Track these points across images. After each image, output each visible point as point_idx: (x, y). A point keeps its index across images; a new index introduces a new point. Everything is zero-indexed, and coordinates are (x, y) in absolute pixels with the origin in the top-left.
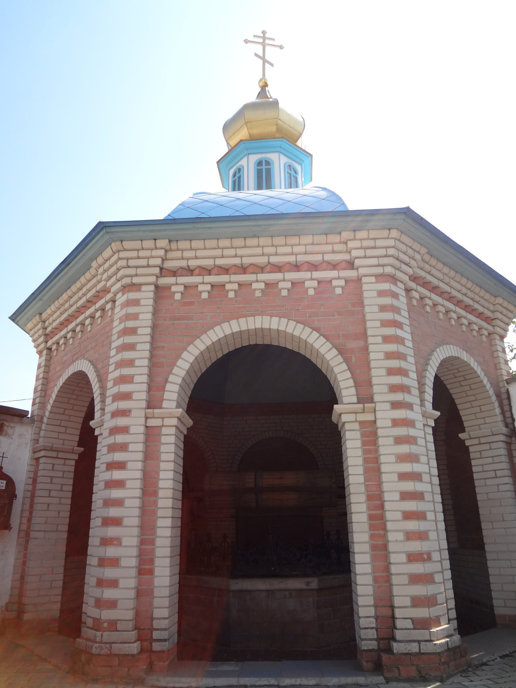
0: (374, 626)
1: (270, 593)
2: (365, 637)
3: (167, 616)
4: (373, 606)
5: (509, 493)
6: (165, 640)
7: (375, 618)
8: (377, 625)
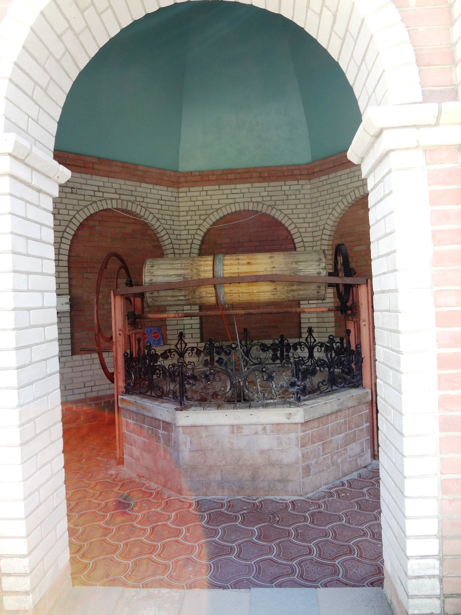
0: (437, 572)
1: (236, 429)
2: (416, 593)
3: (25, 552)
4: (436, 536)
5: (274, 213)
6: (27, 593)
7: (440, 559)
8: (441, 571)
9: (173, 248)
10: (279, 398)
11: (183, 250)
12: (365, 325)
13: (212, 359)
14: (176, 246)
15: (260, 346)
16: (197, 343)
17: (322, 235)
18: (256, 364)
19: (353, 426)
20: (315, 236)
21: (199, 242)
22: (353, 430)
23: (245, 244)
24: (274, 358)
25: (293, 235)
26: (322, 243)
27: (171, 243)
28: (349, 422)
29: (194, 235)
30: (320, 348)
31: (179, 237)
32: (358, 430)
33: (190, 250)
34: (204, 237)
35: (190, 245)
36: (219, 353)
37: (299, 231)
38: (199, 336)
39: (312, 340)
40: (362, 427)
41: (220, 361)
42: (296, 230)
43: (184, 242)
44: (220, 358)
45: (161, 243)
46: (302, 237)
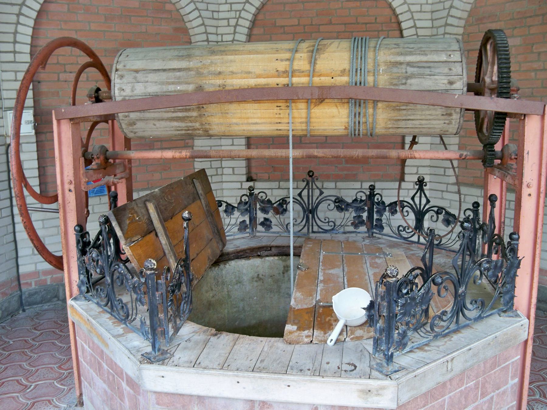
9: (206, 33)
10: (352, 339)
11: (222, 35)
12: (530, 195)
13: (253, 219)
14: (210, 30)
15: (335, 202)
16: (241, 182)
17: (447, 17)
18: (326, 231)
19: (489, 390)
20: (436, 19)
21: (247, 24)
22: (488, 397)
23: (322, 28)
24: (358, 222)
25: (400, 17)
26: (447, 31)
27: (203, 24)
28: (483, 386)
29: (240, 11)
30: (435, 215)
31: (215, 15)
32: (498, 394)
33: (233, 35)
34: (255, 15)
35: (233, 28)
36: (264, 210)
37: (409, 10)
38: (244, 171)
39: (424, 201)
40: (505, 387)
41: (266, 223)
42: (405, 8)
43: (225, 23)
44: (266, 219)
45: (188, 25)
46: (414, 20)
